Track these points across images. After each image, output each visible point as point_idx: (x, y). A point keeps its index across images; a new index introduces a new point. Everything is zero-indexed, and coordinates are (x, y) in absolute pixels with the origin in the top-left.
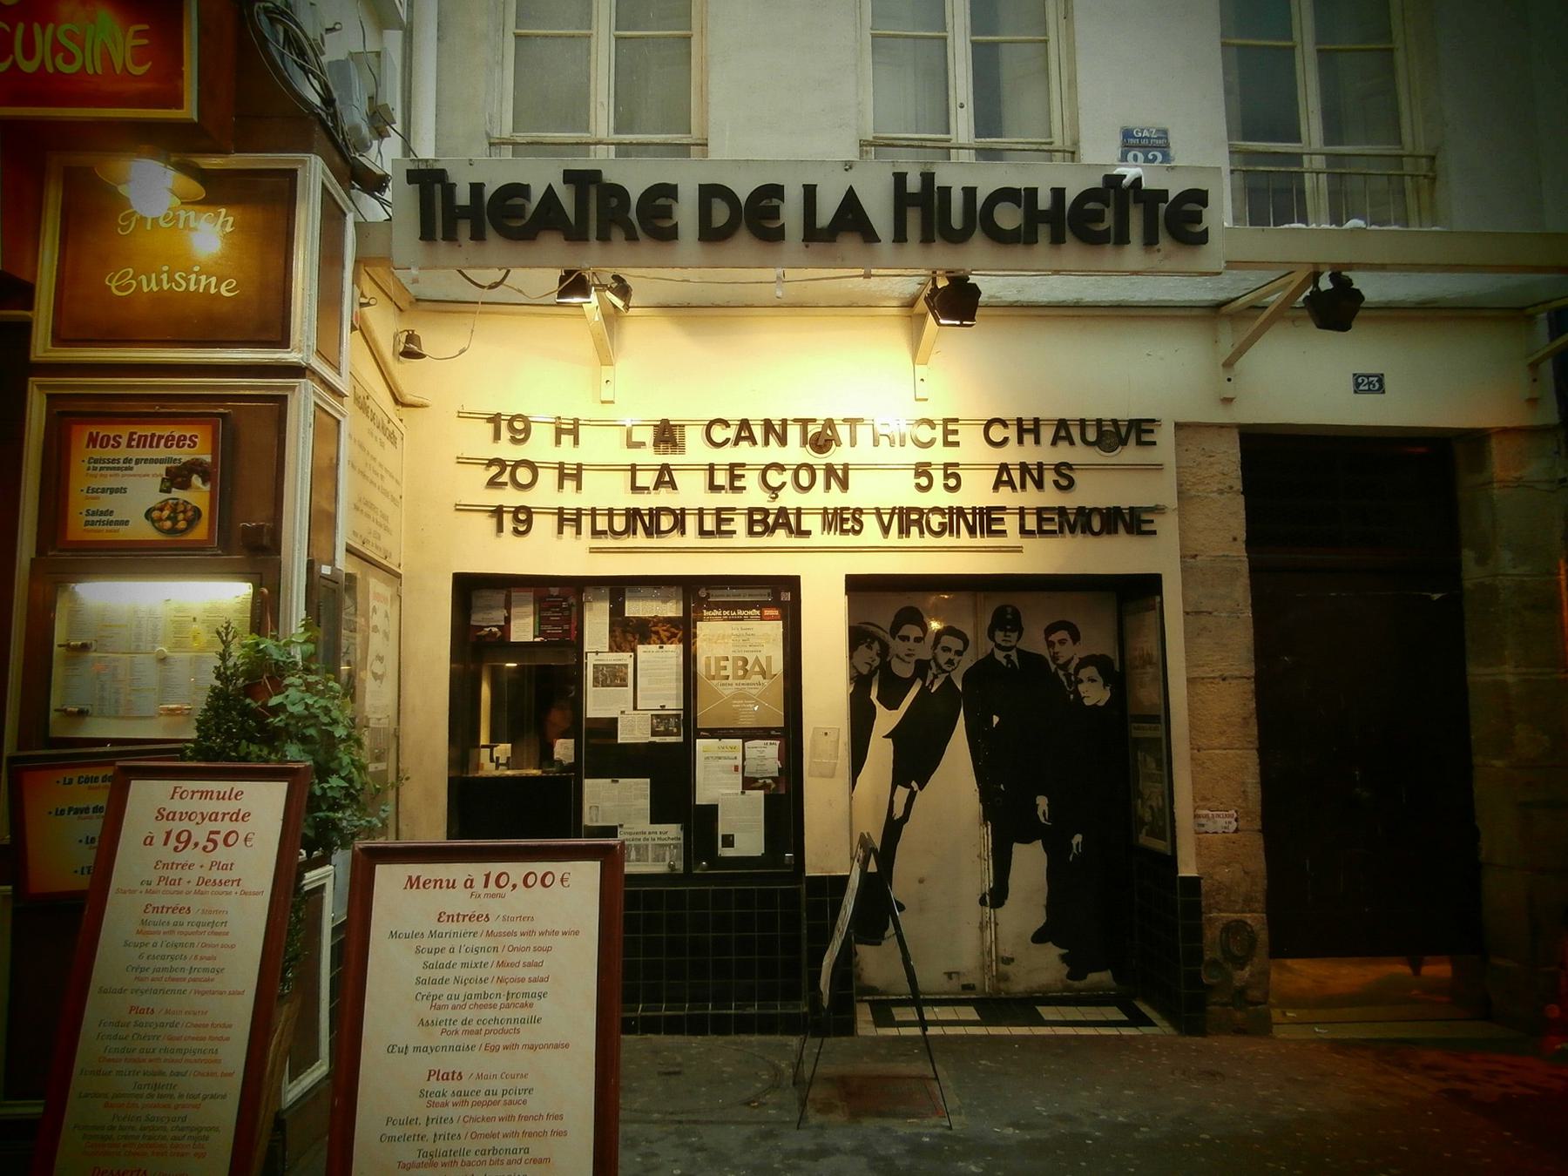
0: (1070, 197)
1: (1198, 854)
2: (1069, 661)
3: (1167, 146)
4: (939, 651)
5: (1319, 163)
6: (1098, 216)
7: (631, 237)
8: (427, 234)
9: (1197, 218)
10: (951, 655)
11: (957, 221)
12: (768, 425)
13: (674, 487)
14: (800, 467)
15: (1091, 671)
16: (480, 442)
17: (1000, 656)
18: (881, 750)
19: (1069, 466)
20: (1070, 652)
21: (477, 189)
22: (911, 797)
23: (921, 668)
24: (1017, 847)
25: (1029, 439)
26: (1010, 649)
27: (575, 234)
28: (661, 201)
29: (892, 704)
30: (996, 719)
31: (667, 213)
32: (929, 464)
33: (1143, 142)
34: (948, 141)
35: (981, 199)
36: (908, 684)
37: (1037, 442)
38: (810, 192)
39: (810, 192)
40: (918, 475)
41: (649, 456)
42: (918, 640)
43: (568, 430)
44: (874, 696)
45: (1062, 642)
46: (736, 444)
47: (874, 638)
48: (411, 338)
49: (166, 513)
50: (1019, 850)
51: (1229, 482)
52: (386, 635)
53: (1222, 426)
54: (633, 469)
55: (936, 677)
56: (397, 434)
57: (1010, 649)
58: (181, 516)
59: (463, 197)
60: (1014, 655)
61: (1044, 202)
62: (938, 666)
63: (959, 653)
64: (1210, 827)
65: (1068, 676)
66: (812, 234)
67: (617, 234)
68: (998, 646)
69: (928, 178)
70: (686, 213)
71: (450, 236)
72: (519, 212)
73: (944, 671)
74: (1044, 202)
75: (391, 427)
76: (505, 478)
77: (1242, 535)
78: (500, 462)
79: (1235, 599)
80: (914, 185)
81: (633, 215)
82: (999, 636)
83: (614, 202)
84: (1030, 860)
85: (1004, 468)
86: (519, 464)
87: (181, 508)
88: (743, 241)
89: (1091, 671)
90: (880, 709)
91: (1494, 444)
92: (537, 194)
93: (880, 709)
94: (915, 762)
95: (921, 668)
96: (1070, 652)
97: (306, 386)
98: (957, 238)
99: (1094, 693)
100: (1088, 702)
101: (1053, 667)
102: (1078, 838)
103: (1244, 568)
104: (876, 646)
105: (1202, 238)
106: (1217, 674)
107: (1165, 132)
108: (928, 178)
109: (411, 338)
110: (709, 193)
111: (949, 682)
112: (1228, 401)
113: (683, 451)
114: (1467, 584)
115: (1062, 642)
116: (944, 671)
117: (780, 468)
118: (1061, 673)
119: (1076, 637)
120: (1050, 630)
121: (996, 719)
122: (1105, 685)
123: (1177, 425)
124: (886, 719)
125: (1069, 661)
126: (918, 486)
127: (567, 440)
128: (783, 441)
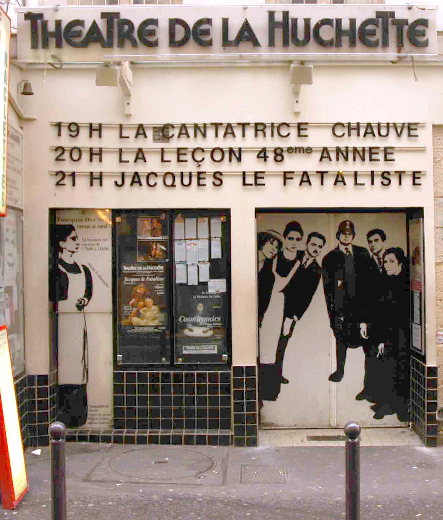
0: (358, 24)
2: (379, 252)
6: (373, 33)
7: (134, 44)
9: (423, 34)
10: (316, 248)
11: (301, 36)
15: (392, 256)
17: (342, 248)
18: (277, 300)
20: (380, 246)
21: (58, 23)
22: (294, 323)
24: (349, 351)
25: (354, 132)
27: (108, 45)
29: (284, 274)
31: (152, 33)
35: (313, 24)
36: (294, 262)
37: (358, 135)
38: (225, 22)
39: (225, 22)
42: (298, 239)
43: (96, 130)
44: (274, 270)
45: (376, 240)
47: (275, 238)
48: (26, 86)
50: (350, 352)
52: (13, 242)
55: (308, 259)
56: (20, 137)
59: (52, 27)
61: (346, 25)
63: (320, 247)
65: (379, 259)
67: (128, 44)
68: (341, 243)
69: (286, 14)
70: (162, 33)
72: (79, 33)
73: (312, 257)
74: (346, 25)
75: (17, 135)
80: (279, 17)
81: (135, 35)
82: (342, 237)
83: (126, 27)
84: (356, 357)
89: (392, 256)
90: (277, 277)
92: (88, 25)
93: (277, 277)
94: (296, 306)
96: (380, 246)
98: (301, 44)
99: (393, 268)
100: (389, 273)
101: (371, 254)
104: (276, 243)
105: (426, 44)
108: (286, 14)
110: (174, 23)
111: (315, 262)
115: (376, 240)
116: (312, 257)
118: (375, 258)
119: (384, 237)
120: (370, 234)
122: (399, 264)
123: (434, 126)
124: (281, 283)
125: (379, 252)
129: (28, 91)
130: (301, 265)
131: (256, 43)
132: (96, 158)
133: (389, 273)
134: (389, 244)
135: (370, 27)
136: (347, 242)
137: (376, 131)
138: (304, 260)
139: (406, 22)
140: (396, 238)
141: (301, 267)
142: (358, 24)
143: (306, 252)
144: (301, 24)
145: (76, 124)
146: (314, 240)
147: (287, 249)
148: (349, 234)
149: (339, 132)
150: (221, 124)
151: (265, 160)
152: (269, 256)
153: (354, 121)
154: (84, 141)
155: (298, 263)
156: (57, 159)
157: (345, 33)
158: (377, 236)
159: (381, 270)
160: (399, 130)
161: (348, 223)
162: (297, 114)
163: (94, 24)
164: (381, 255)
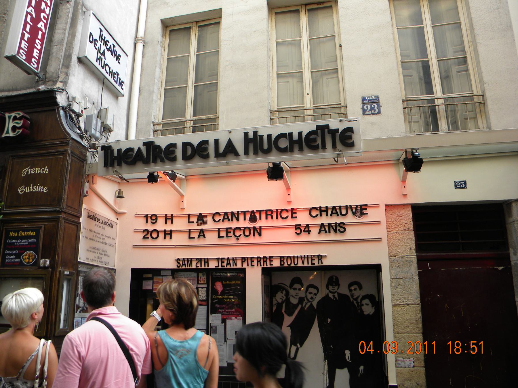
0: (304, 135)
1: (397, 376)
3: (379, 102)
4: (308, 293)
5: (441, 101)
8: (106, 165)
9: (350, 137)
10: (312, 295)
11: (266, 146)
12: (233, 213)
13: (205, 237)
14: (245, 228)
15: (367, 301)
16: (142, 225)
17: (331, 295)
19: (344, 224)
23: (301, 300)
25: (324, 214)
26: (335, 293)
27: (146, 162)
28: (172, 149)
29: (290, 315)
30: (329, 320)
32: (300, 225)
33: (370, 101)
34: (304, 107)
35: (273, 137)
36: (295, 306)
39: (217, 141)
40: (296, 229)
41: (195, 227)
43: (169, 219)
46: (223, 221)
47: (284, 289)
48: (120, 192)
49: (27, 257)
50: (338, 371)
51: (408, 226)
53: (404, 205)
54: (190, 231)
55: (306, 304)
57: (335, 293)
58: (31, 258)
60: (336, 295)
61: (295, 137)
62: (308, 300)
63: (315, 294)
64: (402, 364)
65: (357, 303)
66: (218, 155)
68: (330, 292)
70: (179, 153)
71: (112, 165)
73: (310, 302)
74: (295, 137)
76: (149, 236)
77: (414, 247)
78: (147, 230)
79: (412, 270)
80: (251, 135)
81: (163, 155)
82: (331, 288)
85: (322, 225)
86: (153, 231)
87: (31, 255)
88: (197, 158)
90: (286, 316)
91: (514, 205)
92: (136, 150)
93: (286, 316)
95: (301, 300)
96: (358, 293)
97: (62, 216)
98: (267, 152)
100: (366, 313)
101: (352, 299)
102: (362, 368)
103: (415, 259)
104: (284, 292)
106: (405, 303)
107: (378, 97)
108: (255, 133)
109: (120, 192)
111: (311, 305)
112: (405, 195)
113: (206, 225)
114: (512, 263)
117: (240, 229)
118: (355, 302)
119: (361, 288)
120: (350, 285)
121: (329, 320)
122: (372, 306)
123: (386, 205)
126: (296, 233)
127: (169, 221)
128: (238, 219)
129: (121, 195)
130: (302, 307)
131: (237, 154)
132: (168, 237)
133: (366, 313)
134: (363, 293)
135: (313, 137)
136: (334, 291)
137: (338, 211)
138: (304, 304)
139: (337, 130)
140: (368, 289)
141: (302, 309)
142: (304, 135)
143: (305, 299)
144: (265, 138)
145: (156, 215)
146: (311, 290)
147: (292, 296)
148: (336, 286)
149: (314, 213)
150: (248, 211)
151: (309, 233)
152: (280, 301)
153: (323, 205)
154: (161, 225)
155: (300, 306)
156: (144, 238)
157: (296, 142)
158: (356, 286)
159: (359, 311)
160: (354, 210)
161: (334, 277)
162: (289, 202)
163: (139, 148)
164: (359, 301)
